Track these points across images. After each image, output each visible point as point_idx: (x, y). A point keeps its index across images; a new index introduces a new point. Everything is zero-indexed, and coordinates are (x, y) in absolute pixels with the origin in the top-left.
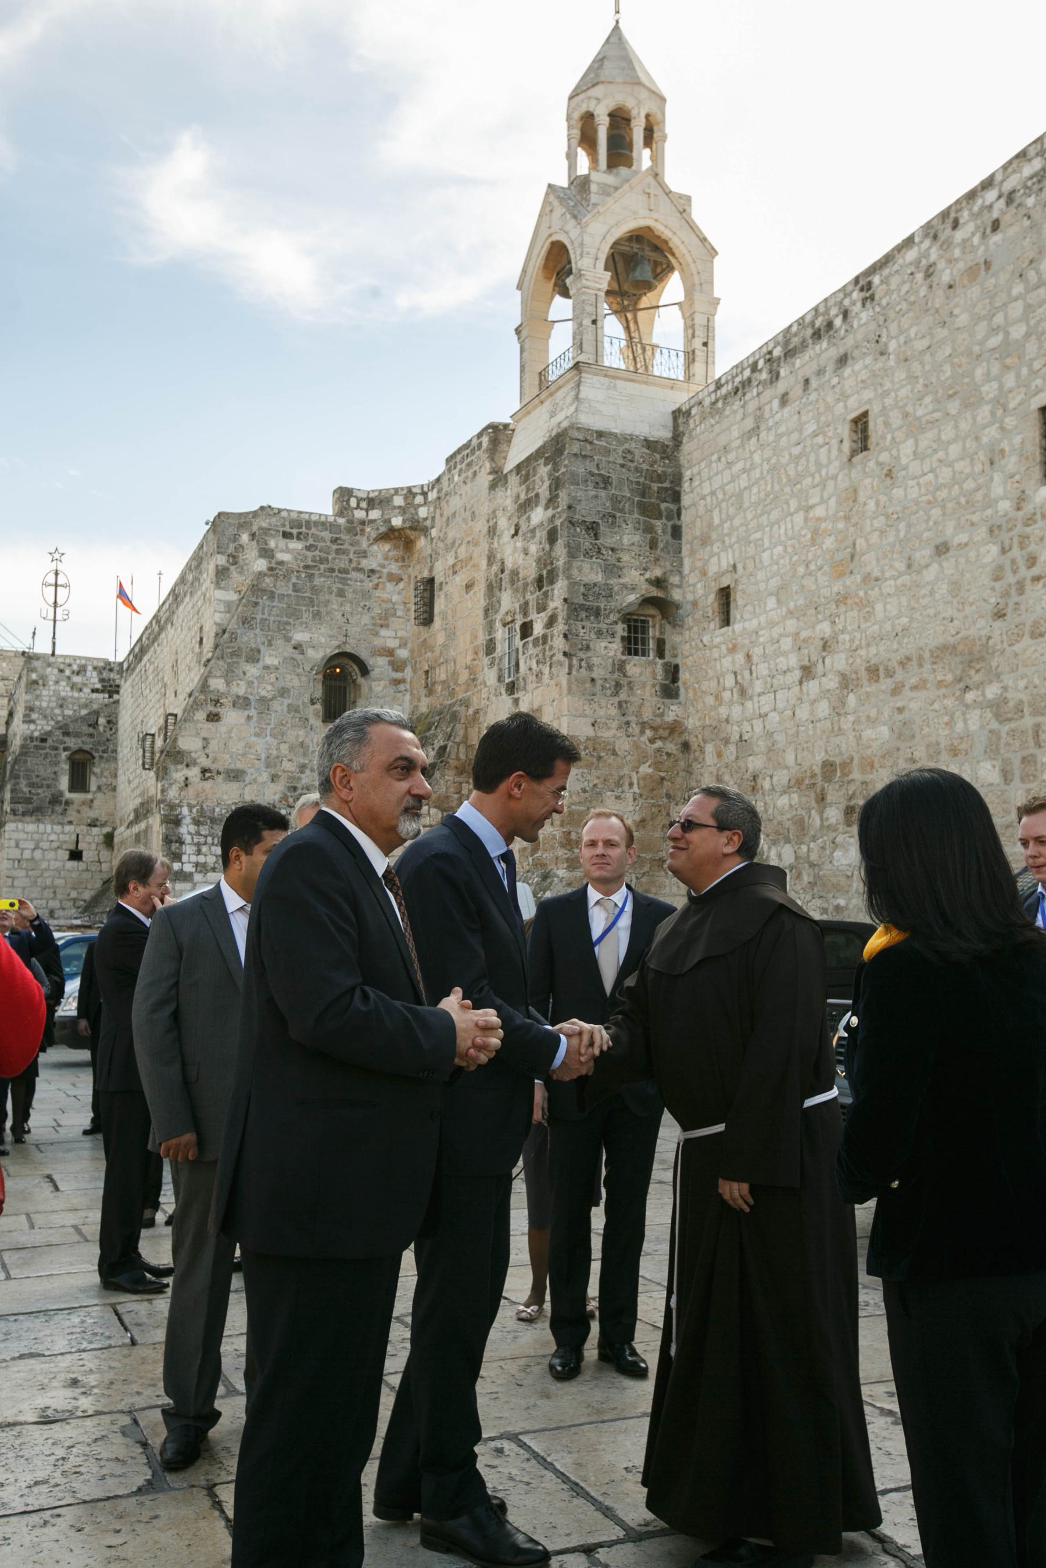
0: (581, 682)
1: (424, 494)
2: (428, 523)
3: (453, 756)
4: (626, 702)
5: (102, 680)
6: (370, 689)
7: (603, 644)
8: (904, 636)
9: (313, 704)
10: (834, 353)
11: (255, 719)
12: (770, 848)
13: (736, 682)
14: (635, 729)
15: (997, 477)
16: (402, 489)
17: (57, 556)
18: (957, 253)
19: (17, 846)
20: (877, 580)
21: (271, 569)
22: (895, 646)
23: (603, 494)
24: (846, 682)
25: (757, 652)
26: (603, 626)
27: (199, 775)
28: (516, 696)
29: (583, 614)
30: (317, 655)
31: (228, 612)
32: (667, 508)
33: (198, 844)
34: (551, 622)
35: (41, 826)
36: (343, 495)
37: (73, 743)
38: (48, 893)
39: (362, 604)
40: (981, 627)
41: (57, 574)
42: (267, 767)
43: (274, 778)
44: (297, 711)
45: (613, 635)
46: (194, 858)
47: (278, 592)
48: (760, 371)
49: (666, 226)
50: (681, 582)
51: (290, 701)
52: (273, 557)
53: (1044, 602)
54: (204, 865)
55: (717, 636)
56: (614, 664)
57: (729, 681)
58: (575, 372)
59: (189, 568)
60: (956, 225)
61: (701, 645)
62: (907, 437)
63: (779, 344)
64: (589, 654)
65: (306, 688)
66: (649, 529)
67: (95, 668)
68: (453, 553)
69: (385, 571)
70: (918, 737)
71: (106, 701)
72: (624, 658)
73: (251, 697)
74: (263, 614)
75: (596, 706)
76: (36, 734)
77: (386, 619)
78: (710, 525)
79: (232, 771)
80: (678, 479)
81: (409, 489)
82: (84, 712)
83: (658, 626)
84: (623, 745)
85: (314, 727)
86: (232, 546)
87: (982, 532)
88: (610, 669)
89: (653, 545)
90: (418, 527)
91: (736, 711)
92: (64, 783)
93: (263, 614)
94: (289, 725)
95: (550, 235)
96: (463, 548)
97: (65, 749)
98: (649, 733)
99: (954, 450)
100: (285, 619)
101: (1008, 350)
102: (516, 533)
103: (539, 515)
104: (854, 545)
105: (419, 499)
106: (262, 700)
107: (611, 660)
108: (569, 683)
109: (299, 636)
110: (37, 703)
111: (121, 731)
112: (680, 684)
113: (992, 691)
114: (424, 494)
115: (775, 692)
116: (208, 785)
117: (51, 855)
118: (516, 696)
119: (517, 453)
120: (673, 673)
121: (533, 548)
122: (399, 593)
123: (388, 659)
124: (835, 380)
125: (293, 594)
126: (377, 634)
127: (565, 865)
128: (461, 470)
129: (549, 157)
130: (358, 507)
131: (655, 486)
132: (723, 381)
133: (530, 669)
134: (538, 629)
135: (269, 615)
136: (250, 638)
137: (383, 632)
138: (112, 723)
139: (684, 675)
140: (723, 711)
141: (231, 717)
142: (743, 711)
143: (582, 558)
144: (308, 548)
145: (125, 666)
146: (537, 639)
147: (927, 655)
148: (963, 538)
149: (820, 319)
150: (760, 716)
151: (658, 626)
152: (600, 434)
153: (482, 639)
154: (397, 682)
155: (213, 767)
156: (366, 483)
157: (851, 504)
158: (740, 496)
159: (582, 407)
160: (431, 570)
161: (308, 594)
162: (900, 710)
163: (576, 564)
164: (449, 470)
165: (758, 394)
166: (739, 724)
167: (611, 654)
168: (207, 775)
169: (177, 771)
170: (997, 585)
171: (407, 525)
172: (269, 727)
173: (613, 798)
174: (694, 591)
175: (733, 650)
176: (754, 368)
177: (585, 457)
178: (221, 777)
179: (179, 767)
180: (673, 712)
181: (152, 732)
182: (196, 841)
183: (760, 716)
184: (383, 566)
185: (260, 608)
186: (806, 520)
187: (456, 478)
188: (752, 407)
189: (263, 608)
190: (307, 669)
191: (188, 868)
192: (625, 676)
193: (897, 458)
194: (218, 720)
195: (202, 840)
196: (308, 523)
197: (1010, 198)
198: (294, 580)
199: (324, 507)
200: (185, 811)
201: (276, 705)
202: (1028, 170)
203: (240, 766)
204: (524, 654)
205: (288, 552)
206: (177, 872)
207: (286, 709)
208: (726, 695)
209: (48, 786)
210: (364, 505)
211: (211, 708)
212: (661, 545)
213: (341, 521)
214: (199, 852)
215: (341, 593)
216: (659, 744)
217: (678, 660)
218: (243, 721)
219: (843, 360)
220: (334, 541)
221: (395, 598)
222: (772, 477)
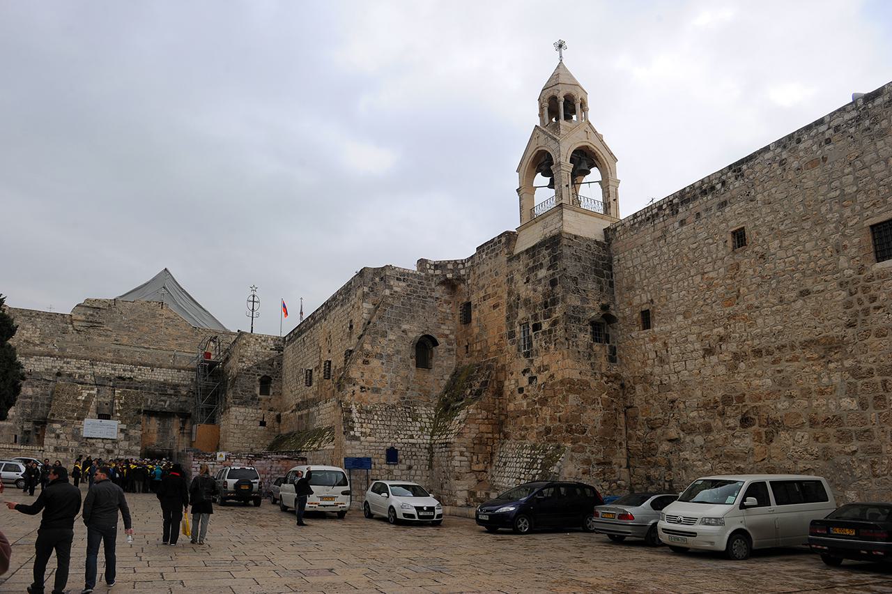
1: (463, 264)
2: (466, 277)
3: (491, 386)
4: (594, 363)
5: (275, 345)
7: (582, 335)
8: (779, 335)
10: (717, 201)
13: (657, 356)
14: (598, 376)
15: (842, 259)
16: (452, 261)
17: (254, 289)
18: (801, 154)
19: (236, 418)
20: (758, 307)
21: (391, 294)
22: (773, 340)
23: (578, 264)
24: (736, 357)
25: (671, 341)
28: (531, 358)
29: (573, 320)
30: (415, 335)
31: (369, 313)
32: (607, 273)
33: (361, 423)
34: (555, 323)
35: (247, 409)
36: (422, 263)
37: (262, 373)
38: (250, 440)
40: (837, 332)
41: (254, 296)
43: (394, 392)
45: (587, 331)
46: (360, 430)
48: (665, 210)
49: (593, 144)
52: (392, 289)
53: (879, 320)
54: (365, 433)
55: (637, 332)
56: (588, 345)
57: (652, 355)
58: (559, 208)
59: (339, 293)
60: (799, 141)
62: (774, 239)
63: (677, 197)
65: (407, 351)
66: (599, 282)
67: (272, 339)
68: (483, 291)
69: (443, 298)
70: (794, 386)
71: (277, 354)
76: (245, 368)
78: (633, 281)
80: (611, 260)
81: (455, 261)
82: (267, 359)
84: (593, 384)
86: (371, 283)
87: (835, 284)
89: (601, 290)
90: (461, 279)
91: (657, 370)
92: (258, 390)
95: (538, 148)
96: (490, 289)
97: (258, 375)
98: (605, 379)
99: (809, 246)
100: (398, 318)
101: (842, 199)
102: (528, 281)
103: (542, 273)
104: (739, 291)
105: (460, 266)
106: (388, 355)
109: (405, 327)
110: (246, 354)
111: (284, 368)
113: (848, 363)
114: (463, 264)
116: (363, 394)
117: (252, 423)
118: (531, 358)
119: (522, 245)
120: (613, 350)
121: (540, 289)
124: (719, 213)
126: (440, 328)
128: (487, 253)
129: (530, 116)
130: (430, 268)
131: (601, 262)
132: (638, 215)
133: (541, 346)
134: (545, 326)
136: (381, 326)
137: (443, 327)
138: (280, 364)
140: (648, 370)
141: (375, 363)
144: (408, 286)
145: (287, 339)
146: (545, 331)
147: (797, 344)
148: (820, 287)
149: (706, 185)
152: (576, 237)
153: (505, 331)
154: (450, 350)
155: (366, 386)
156: (434, 257)
157: (736, 271)
158: (655, 267)
159: (564, 224)
160: (468, 298)
162: (779, 371)
164: (479, 253)
165: (664, 221)
169: (349, 387)
170: (848, 311)
171: (455, 277)
174: (625, 310)
175: (655, 340)
176: (660, 208)
177: (570, 246)
179: (350, 385)
181: (310, 368)
184: (442, 296)
186: (702, 278)
187: (484, 256)
188: (659, 226)
191: (358, 434)
193: (768, 249)
195: (363, 421)
196: (408, 274)
197: (837, 129)
198: (402, 300)
199: (412, 267)
200: (353, 406)
201: (394, 358)
202: (847, 117)
203: (378, 386)
205: (399, 287)
206: (352, 436)
208: (650, 362)
209: (250, 392)
210: (433, 267)
212: (605, 290)
213: (423, 274)
214: (362, 427)
215: (423, 307)
216: (610, 384)
219: (723, 204)
220: (420, 283)
222: (677, 258)
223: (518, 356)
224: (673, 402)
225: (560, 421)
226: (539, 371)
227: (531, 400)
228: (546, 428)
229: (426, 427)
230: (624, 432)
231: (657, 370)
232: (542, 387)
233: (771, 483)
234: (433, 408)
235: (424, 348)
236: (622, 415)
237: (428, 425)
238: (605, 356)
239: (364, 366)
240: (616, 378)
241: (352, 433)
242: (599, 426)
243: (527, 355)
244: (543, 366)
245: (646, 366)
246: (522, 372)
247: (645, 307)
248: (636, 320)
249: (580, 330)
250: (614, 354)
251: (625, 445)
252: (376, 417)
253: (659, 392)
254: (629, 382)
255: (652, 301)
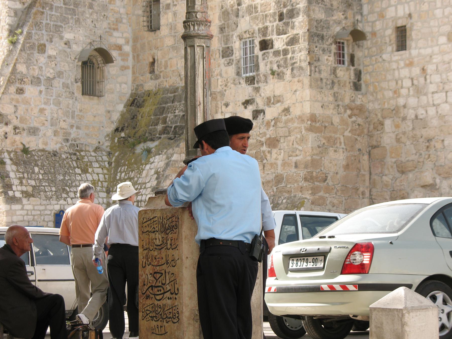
0: (317, 80)
4: (337, 93)
6: (109, 72)
7: (326, 57)
9: (77, 82)
11: (43, 93)
12: (441, 182)
13: (413, 84)
25: (430, 68)
26: (325, 46)
27: (13, 131)
28: (256, 85)
29: (316, 39)
34: (293, 41)
39: (103, 14)
42: (52, 126)
43: (56, 133)
44: (68, 87)
45: (330, 52)
47: (55, 5)
50: (362, 19)
51: (63, 80)
55: (390, 55)
56: (331, 70)
57: (407, 83)
61: (380, 60)
64: (319, 63)
65: (73, 71)
72: (336, 66)
73: (41, 78)
74: (47, 20)
75: (323, 95)
77: (117, 25)
79: (32, 128)
83: (351, 47)
84: (336, 120)
85: (78, 98)
88: (329, 73)
91: (412, 101)
93: (47, 20)
94: (64, 97)
98: (349, 112)
107: (329, 67)
108: (311, 81)
109: (68, 36)
112: (362, 82)
115: (447, 92)
118: (256, 85)
122: (124, 7)
123: (119, 52)
125: (64, 6)
126: (111, 35)
127: (310, 192)
135: (50, 20)
137: (116, 34)
139: (364, 77)
140: (401, 101)
141: (31, 91)
142: (418, 102)
143: (314, 4)
150: (434, 105)
151: (351, 47)
155: (20, 125)
161: (72, 7)
163: (312, 7)
166: (414, 109)
167: (330, 63)
168: (17, 131)
172: (52, 98)
173: (333, 151)
175: (410, 64)
178: (26, 132)
180: (359, 100)
182: (18, 176)
183: (434, 105)
185: (45, 16)
189: (47, 16)
190: (73, 58)
191: (18, 195)
192: (336, 77)
194: (22, 93)
204: (264, 59)
207: (61, 85)
208: (404, 92)
211: (18, 85)
214: (21, 183)
216: (354, 119)
217: (361, 68)
218: (37, 93)
221: (122, 11)
223: (237, 82)
224: (429, 140)
225: (296, 167)
226: (269, 102)
227: (255, 141)
228: (277, 176)
229: (99, 180)
230: (367, 178)
231: (412, 101)
232: (273, 123)
233: (301, 216)
234: (104, 153)
235: (92, 66)
236: (366, 157)
237: (101, 177)
238: (350, 83)
239: (18, 96)
240: (360, 110)
241: (11, 193)
242: (342, 173)
243: (251, 81)
244: (274, 96)
245: (399, 96)
246: (243, 104)
247: (400, 23)
248: (389, 36)
249: (324, 50)
250: (359, 80)
251: (367, 194)
252: (36, 169)
253: (413, 129)
254: (376, 115)
255: (410, 15)
